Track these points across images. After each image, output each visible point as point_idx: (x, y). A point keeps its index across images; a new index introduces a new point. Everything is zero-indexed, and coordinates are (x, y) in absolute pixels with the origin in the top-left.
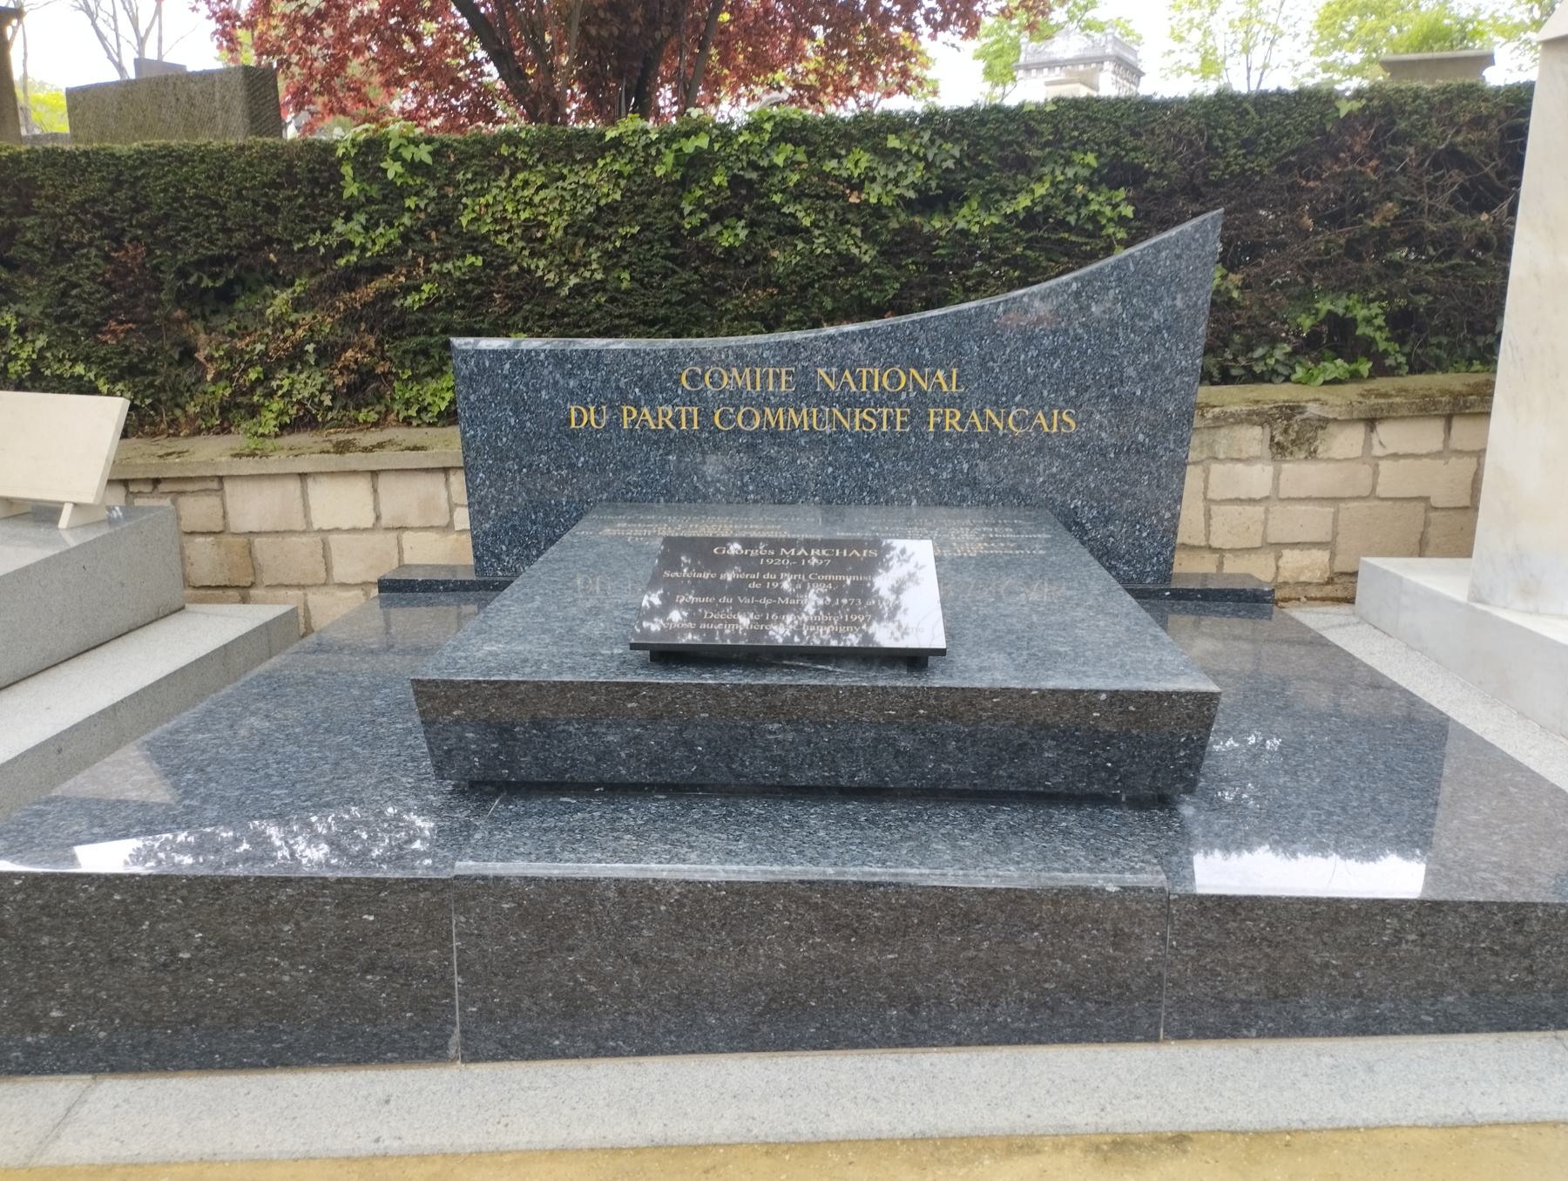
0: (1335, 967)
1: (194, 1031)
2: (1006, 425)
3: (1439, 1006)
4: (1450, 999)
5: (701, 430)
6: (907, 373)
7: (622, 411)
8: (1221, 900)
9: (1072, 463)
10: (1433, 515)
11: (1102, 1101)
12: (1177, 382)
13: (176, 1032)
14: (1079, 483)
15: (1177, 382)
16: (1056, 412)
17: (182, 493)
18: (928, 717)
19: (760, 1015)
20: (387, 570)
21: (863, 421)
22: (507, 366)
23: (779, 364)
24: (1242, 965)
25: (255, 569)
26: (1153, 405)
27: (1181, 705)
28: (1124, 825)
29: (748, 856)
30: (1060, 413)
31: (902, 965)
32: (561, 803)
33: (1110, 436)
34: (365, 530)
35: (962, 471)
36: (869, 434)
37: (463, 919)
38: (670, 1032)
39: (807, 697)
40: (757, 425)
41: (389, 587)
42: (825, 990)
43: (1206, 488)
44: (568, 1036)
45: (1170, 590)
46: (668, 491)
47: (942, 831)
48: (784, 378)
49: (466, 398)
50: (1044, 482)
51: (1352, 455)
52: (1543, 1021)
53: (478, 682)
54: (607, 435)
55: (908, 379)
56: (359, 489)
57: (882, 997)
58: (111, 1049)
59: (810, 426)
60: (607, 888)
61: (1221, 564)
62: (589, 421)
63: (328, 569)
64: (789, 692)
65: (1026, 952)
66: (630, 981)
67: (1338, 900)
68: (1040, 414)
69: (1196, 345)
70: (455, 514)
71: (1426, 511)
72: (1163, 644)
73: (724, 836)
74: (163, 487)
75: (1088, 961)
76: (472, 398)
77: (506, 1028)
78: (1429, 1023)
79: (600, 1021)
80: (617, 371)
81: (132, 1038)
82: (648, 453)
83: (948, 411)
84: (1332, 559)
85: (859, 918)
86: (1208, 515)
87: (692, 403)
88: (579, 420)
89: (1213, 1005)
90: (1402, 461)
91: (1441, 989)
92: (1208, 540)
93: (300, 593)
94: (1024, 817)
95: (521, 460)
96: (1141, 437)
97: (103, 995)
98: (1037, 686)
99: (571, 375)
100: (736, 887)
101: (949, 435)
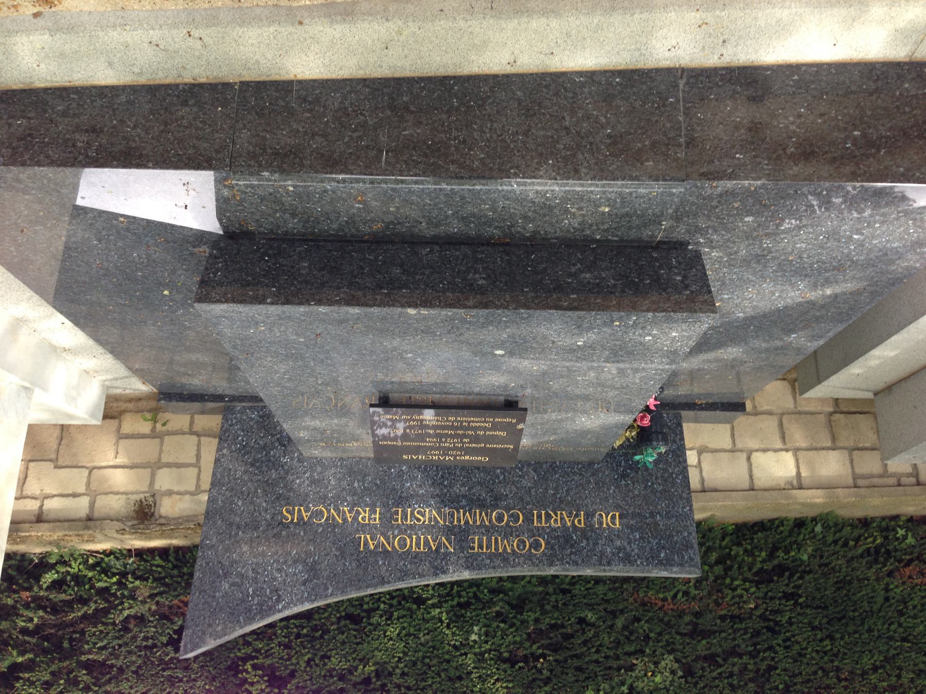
0: (129, 126)
1: (849, 87)
2: (328, 511)
3: (66, 104)
4: (59, 108)
5: (532, 510)
6: (393, 547)
7: (585, 523)
8: (198, 167)
9: (285, 486)
10: (53, 456)
11: (276, 42)
12: (214, 540)
13: (860, 86)
14: (282, 472)
15: (214, 540)
16: (295, 520)
17: (881, 476)
18: (382, 288)
19: (489, 97)
20: (741, 420)
21: (423, 515)
22: (662, 555)
23: (478, 554)
24: (186, 127)
25: (830, 424)
26: (231, 524)
27: (219, 294)
28: (257, 220)
29: (496, 195)
30: (293, 519)
31: (399, 127)
32: (617, 236)
33: (260, 504)
34: (757, 451)
35: (359, 481)
36: (420, 507)
37: (679, 155)
38: (546, 87)
39: (460, 300)
40: (494, 514)
41: (738, 407)
42: (448, 112)
43: (199, 475)
44: (610, 84)
45: (225, 401)
46: (554, 469)
47: (372, 215)
48: (476, 545)
49: (690, 534)
50: (304, 473)
51: (103, 497)
52: (4, 96)
53: (673, 311)
54: (595, 507)
55: (393, 543)
56: (761, 479)
57: (412, 108)
58: (900, 77)
59: (458, 512)
60: (586, 174)
61: (192, 422)
62: (607, 517)
63: (781, 425)
64: (471, 303)
65: (322, 135)
66: (572, 118)
67: (124, 167)
68: (306, 519)
69: (201, 565)
70: (696, 461)
71: (57, 459)
72: (230, 342)
73: (512, 210)
74: (893, 481)
75: (283, 130)
76: (686, 534)
77: (650, 89)
78: (73, 93)
79: (590, 93)
80: (588, 551)
81: (887, 83)
82: (567, 495)
83: (367, 522)
84: (120, 427)
85: (426, 156)
86: (198, 457)
87: (538, 528)
88: (613, 517)
89: (205, 103)
90: (70, 492)
91: (65, 114)
92: (199, 440)
93: (799, 409)
94: (320, 226)
95: (652, 491)
96: (240, 503)
97: (907, 109)
98: (311, 307)
99: (620, 549)
100: (504, 174)
101: (367, 506)
